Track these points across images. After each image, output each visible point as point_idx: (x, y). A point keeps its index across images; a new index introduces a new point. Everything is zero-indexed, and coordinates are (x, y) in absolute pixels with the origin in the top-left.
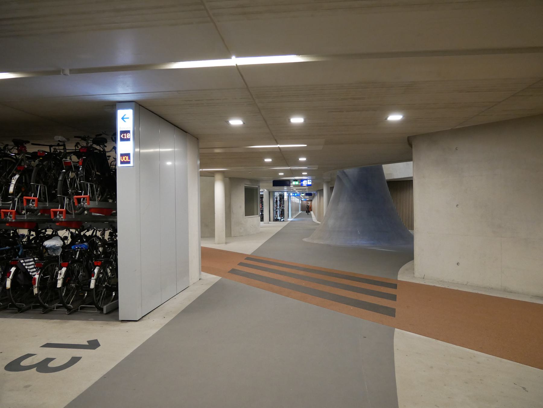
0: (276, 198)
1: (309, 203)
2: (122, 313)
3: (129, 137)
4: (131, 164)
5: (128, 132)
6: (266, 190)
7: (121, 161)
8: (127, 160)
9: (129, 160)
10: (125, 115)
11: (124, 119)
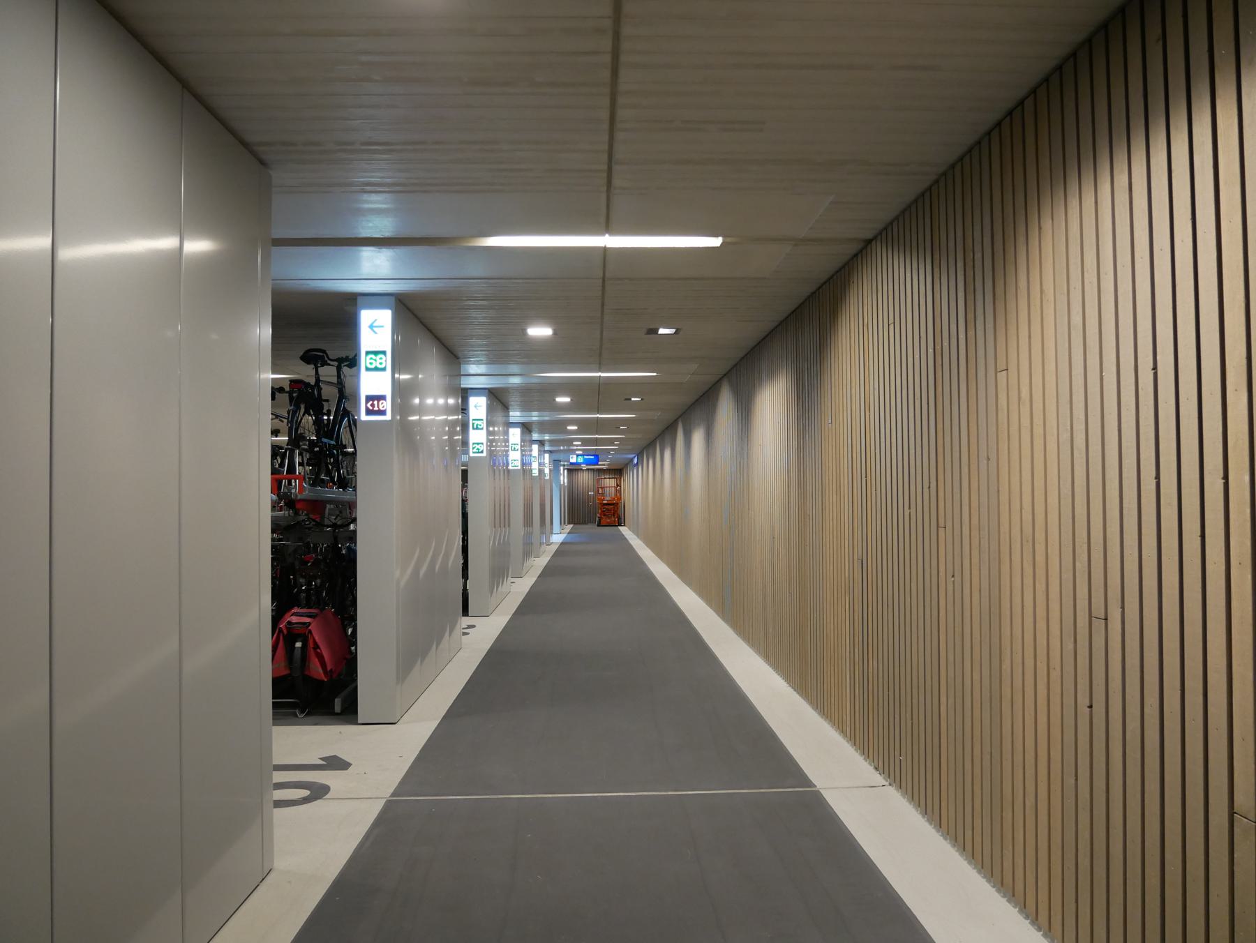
1: (610, 482)
2: (362, 714)
3: (383, 407)
5: (381, 398)
10: (376, 320)
11: (374, 329)
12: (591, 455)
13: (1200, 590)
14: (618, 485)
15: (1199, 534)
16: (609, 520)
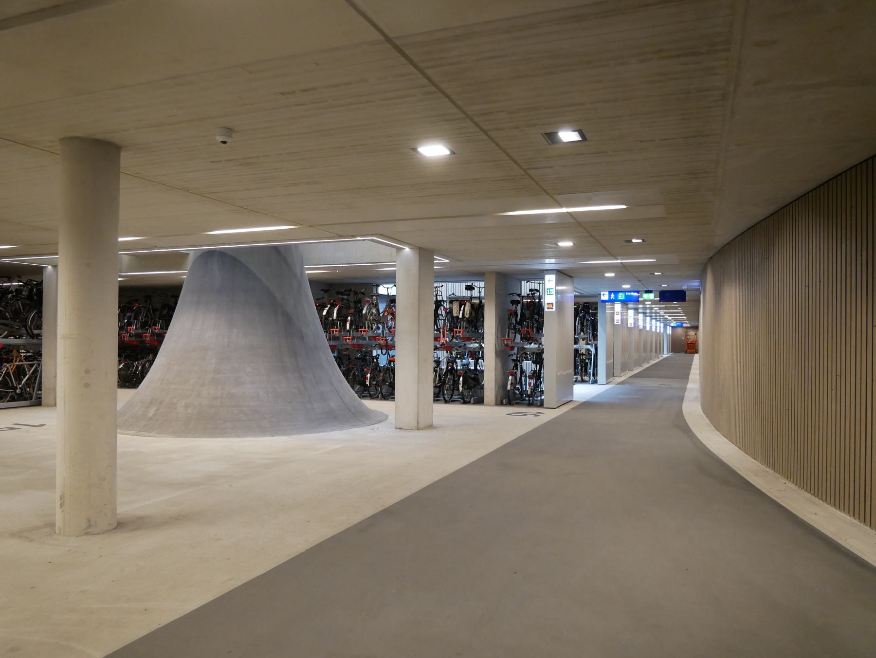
6: (407, 249)
14: (696, 334)
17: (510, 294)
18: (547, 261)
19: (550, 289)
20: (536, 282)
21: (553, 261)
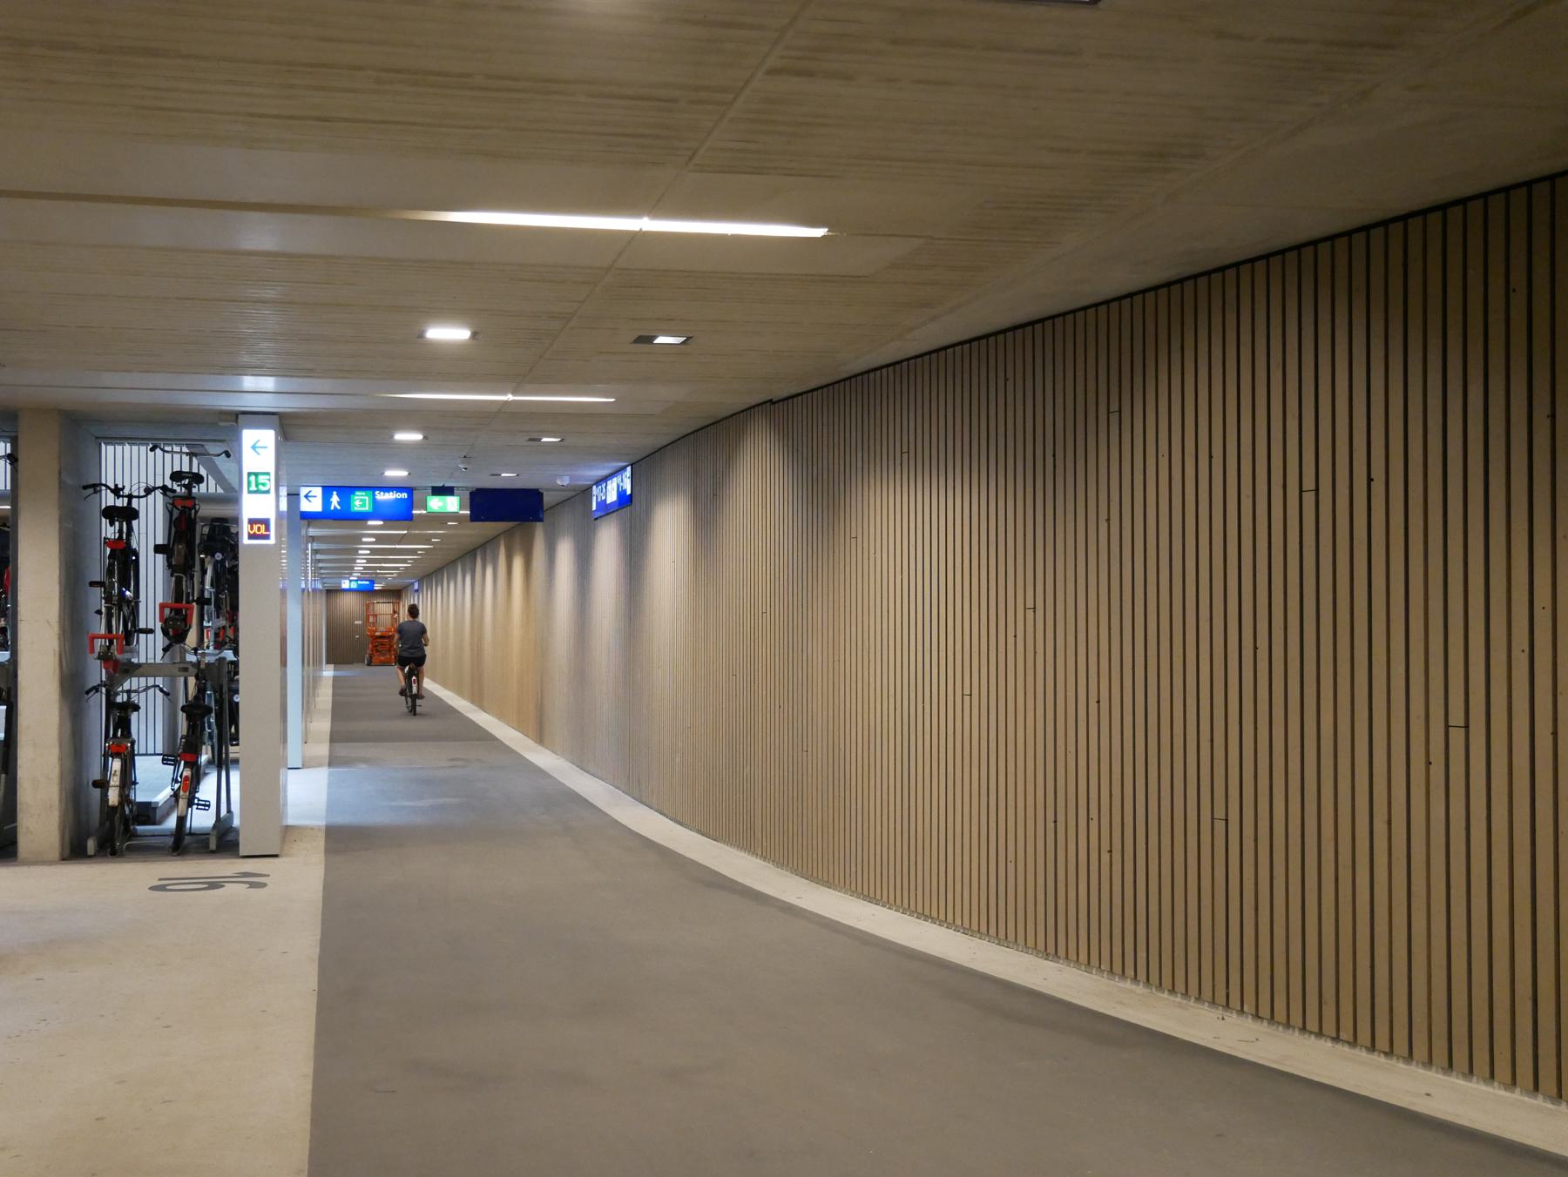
0: (111, 513)
4: (272, 541)
7: (249, 533)
8: (263, 531)
9: (267, 533)
12: (366, 580)
13: (1406, 963)
14: (395, 612)
15: (1531, 995)
16: (383, 658)
17: (85, 488)
18: (249, 382)
19: (256, 474)
20: (177, 449)
21: (268, 383)
